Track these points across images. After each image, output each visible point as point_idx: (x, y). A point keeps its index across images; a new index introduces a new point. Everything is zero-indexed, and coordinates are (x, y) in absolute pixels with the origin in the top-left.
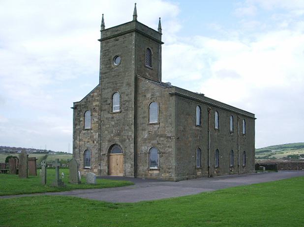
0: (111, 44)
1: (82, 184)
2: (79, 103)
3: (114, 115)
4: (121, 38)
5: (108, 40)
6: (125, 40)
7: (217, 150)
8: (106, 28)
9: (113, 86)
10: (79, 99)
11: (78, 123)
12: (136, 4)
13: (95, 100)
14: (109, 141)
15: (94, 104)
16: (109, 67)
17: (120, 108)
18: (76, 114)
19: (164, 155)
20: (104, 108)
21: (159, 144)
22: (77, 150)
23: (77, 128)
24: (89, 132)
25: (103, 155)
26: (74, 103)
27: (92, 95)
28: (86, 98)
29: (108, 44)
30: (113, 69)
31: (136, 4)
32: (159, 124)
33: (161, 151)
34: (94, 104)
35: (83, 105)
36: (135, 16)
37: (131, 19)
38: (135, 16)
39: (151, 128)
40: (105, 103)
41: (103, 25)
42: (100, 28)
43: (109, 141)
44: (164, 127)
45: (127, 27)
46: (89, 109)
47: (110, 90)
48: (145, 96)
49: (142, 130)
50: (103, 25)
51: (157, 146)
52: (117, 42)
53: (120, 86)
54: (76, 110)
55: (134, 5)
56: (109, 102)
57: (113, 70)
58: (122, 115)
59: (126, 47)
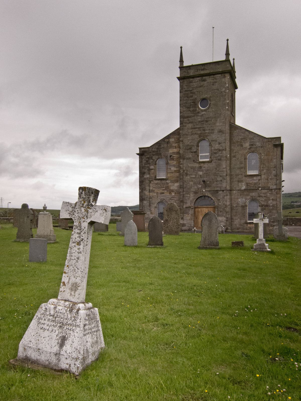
0: (195, 85)
1: (270, 206)
2: (147, 150)
3: (202, 165)
4: (209, 80)
5: (191, 79)
6: (216, 82)
7: (65, 291)
8: (185, 64)
9: (199, 132)
10: (148, 144)
11: (146, 171)
12: (228, 40)
13: (171, 147)
14: (196, 193)
15: (171, 151)
16: (193, 111)
17: (210, 158)
18: (144, 162)
19: (266, 208)
20: (187, 157)
21: (259, 196)
22: (145, 202)
23: (145, 177)
24: (164, 182)
25: (186, 208)
26: (140, 149)
27: (167, 140)
28: (158, 144)
29: (191, 84)
30: (199, 113)
31: (228, 40)
32: (261, 176)
33: (263, 204)
34: (171, 151)
35: (154, 152)
36: (227, 54)
37: (223, 58)
38: (227, 54)
39: (249, 180)
40: (189, 151)
41: (181, 61)
42: (178, 64)
43: (196, 193)
44: (267, 179)
45: (218, 66)
46: (163, 156)
47: (197, 136)
48: (242, 146)
49: (239, 181)
50: (181, 61)
51: (258, 198)
52: (203, 83)
53: (209, 133)
54: (143, 157)
55: (226, 42)
56: (194, 149)
57: (198, 114)
58: (213, 165)
59: (218, 89)
